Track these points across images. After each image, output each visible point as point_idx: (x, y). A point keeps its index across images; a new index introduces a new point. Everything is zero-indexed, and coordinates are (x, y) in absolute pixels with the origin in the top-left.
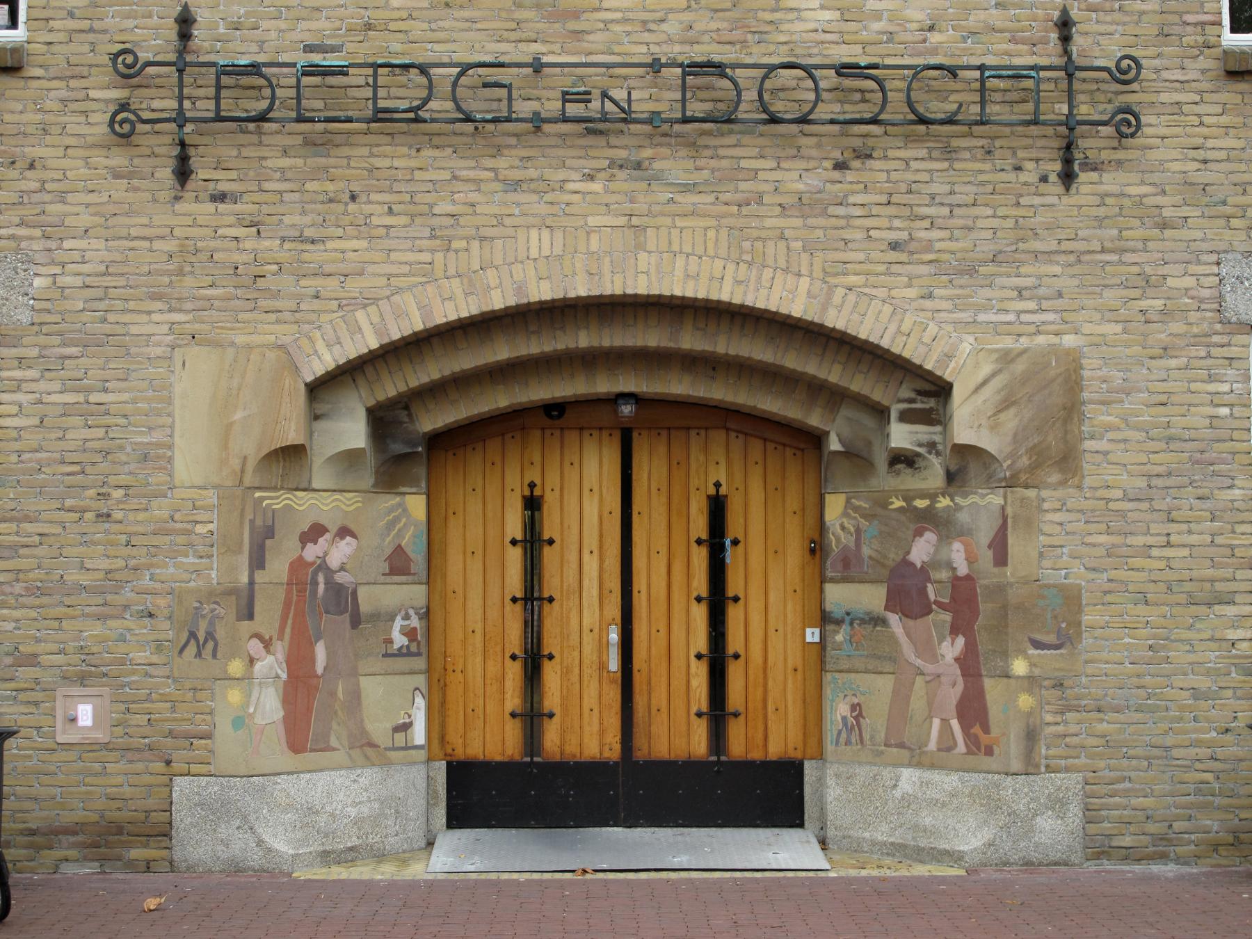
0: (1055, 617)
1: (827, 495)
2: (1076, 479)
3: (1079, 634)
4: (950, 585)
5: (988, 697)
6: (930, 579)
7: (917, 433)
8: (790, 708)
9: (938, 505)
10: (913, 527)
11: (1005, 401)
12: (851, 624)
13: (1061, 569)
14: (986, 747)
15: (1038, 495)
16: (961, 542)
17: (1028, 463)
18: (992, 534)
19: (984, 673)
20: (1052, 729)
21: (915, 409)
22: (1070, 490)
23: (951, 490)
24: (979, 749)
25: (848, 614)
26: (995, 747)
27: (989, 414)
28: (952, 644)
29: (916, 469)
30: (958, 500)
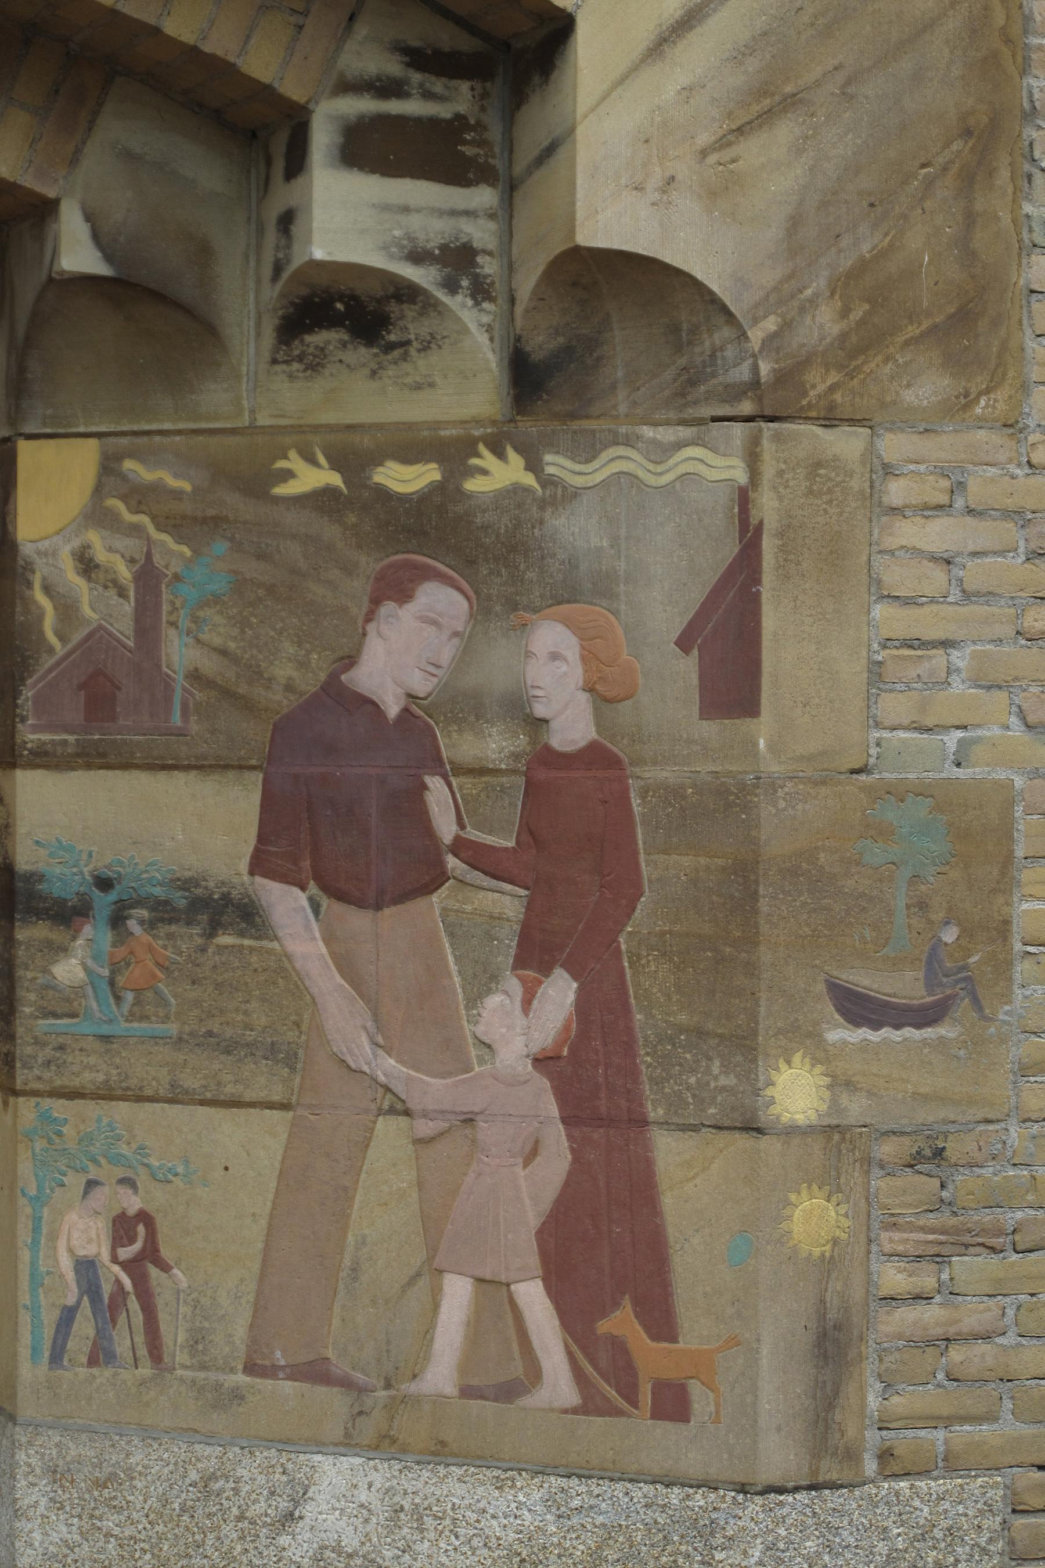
0: (922, 905)
1: (24, 447)
2: (1001, 395)
3: (1003, 967)
4: (521, 781)
5: (668, 1201)
6: (439, 760)
7: (406, 209)
9: (473, 485)
10: (370, 564)
11: (763, 92)
12: (117, 920)
13: (946, 728)
14: (660, 1387)
15: (871, 450)
16: (567, 622)
17: (835, 329)
18: (696, 595)
19: (655, 1112)
20: (907, 1316)
21: (401, 121)
22: (981, 434)
23: (529, 427)
24: (632, 1400)
25: (104, 884)
26: (695, 1388)
27: (704, 139)
28: (527, 1003)
29: (390, 347)
30: (556, 464)
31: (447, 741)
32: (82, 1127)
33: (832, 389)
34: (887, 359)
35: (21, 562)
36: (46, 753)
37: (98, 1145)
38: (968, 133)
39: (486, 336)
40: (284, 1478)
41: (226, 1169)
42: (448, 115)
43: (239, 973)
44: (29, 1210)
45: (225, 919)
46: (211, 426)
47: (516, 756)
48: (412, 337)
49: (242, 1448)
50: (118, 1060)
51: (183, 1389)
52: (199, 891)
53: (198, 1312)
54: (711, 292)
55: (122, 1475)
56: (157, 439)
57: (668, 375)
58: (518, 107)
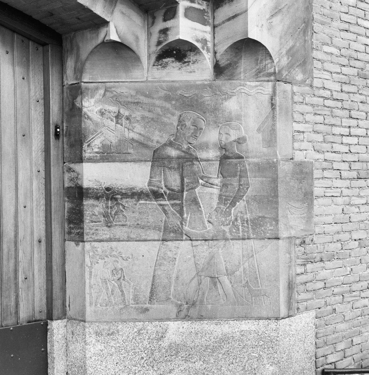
8: (36, 276)
11: (276, 8)
17: (286, 63)
29: (185, 62)
31: (199, 154)
32: (103, 249)
33: (286, 75)
34: (294, 70)
35: (83, 113)
36: (91, 159)
37: (108, 253)
38: (305, 22)
39: (209, 61)
40: (160, 328)
41: (143, 256)
42: (202, 9)
43: (146, 209)
44: (88, 270)
45: (141, 197)
46: (137, 80)
47: (217, 157)
48: (191, 60)
49: (149, 322)
50: (113, 232)
51: (132, 309)
52: (134, 191)
53: (136, 290)
54: (268, 51)
55: (116, 332)
56: (121, 83)
57: (254, 70)
58: (217, 8)
